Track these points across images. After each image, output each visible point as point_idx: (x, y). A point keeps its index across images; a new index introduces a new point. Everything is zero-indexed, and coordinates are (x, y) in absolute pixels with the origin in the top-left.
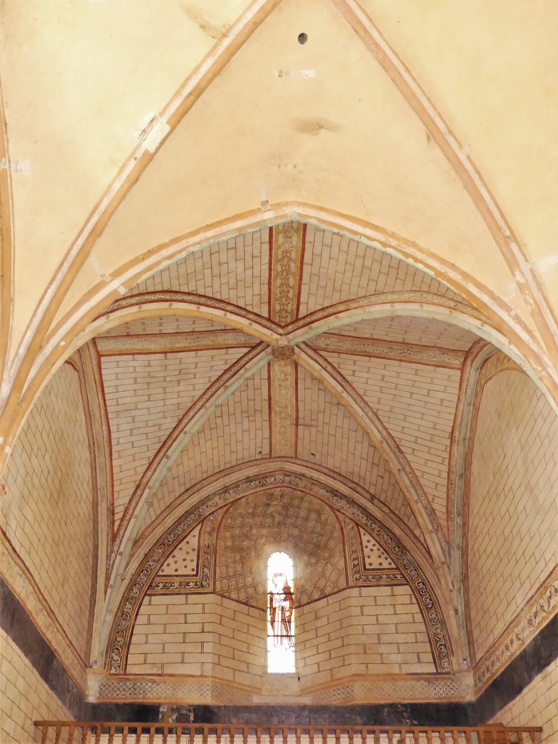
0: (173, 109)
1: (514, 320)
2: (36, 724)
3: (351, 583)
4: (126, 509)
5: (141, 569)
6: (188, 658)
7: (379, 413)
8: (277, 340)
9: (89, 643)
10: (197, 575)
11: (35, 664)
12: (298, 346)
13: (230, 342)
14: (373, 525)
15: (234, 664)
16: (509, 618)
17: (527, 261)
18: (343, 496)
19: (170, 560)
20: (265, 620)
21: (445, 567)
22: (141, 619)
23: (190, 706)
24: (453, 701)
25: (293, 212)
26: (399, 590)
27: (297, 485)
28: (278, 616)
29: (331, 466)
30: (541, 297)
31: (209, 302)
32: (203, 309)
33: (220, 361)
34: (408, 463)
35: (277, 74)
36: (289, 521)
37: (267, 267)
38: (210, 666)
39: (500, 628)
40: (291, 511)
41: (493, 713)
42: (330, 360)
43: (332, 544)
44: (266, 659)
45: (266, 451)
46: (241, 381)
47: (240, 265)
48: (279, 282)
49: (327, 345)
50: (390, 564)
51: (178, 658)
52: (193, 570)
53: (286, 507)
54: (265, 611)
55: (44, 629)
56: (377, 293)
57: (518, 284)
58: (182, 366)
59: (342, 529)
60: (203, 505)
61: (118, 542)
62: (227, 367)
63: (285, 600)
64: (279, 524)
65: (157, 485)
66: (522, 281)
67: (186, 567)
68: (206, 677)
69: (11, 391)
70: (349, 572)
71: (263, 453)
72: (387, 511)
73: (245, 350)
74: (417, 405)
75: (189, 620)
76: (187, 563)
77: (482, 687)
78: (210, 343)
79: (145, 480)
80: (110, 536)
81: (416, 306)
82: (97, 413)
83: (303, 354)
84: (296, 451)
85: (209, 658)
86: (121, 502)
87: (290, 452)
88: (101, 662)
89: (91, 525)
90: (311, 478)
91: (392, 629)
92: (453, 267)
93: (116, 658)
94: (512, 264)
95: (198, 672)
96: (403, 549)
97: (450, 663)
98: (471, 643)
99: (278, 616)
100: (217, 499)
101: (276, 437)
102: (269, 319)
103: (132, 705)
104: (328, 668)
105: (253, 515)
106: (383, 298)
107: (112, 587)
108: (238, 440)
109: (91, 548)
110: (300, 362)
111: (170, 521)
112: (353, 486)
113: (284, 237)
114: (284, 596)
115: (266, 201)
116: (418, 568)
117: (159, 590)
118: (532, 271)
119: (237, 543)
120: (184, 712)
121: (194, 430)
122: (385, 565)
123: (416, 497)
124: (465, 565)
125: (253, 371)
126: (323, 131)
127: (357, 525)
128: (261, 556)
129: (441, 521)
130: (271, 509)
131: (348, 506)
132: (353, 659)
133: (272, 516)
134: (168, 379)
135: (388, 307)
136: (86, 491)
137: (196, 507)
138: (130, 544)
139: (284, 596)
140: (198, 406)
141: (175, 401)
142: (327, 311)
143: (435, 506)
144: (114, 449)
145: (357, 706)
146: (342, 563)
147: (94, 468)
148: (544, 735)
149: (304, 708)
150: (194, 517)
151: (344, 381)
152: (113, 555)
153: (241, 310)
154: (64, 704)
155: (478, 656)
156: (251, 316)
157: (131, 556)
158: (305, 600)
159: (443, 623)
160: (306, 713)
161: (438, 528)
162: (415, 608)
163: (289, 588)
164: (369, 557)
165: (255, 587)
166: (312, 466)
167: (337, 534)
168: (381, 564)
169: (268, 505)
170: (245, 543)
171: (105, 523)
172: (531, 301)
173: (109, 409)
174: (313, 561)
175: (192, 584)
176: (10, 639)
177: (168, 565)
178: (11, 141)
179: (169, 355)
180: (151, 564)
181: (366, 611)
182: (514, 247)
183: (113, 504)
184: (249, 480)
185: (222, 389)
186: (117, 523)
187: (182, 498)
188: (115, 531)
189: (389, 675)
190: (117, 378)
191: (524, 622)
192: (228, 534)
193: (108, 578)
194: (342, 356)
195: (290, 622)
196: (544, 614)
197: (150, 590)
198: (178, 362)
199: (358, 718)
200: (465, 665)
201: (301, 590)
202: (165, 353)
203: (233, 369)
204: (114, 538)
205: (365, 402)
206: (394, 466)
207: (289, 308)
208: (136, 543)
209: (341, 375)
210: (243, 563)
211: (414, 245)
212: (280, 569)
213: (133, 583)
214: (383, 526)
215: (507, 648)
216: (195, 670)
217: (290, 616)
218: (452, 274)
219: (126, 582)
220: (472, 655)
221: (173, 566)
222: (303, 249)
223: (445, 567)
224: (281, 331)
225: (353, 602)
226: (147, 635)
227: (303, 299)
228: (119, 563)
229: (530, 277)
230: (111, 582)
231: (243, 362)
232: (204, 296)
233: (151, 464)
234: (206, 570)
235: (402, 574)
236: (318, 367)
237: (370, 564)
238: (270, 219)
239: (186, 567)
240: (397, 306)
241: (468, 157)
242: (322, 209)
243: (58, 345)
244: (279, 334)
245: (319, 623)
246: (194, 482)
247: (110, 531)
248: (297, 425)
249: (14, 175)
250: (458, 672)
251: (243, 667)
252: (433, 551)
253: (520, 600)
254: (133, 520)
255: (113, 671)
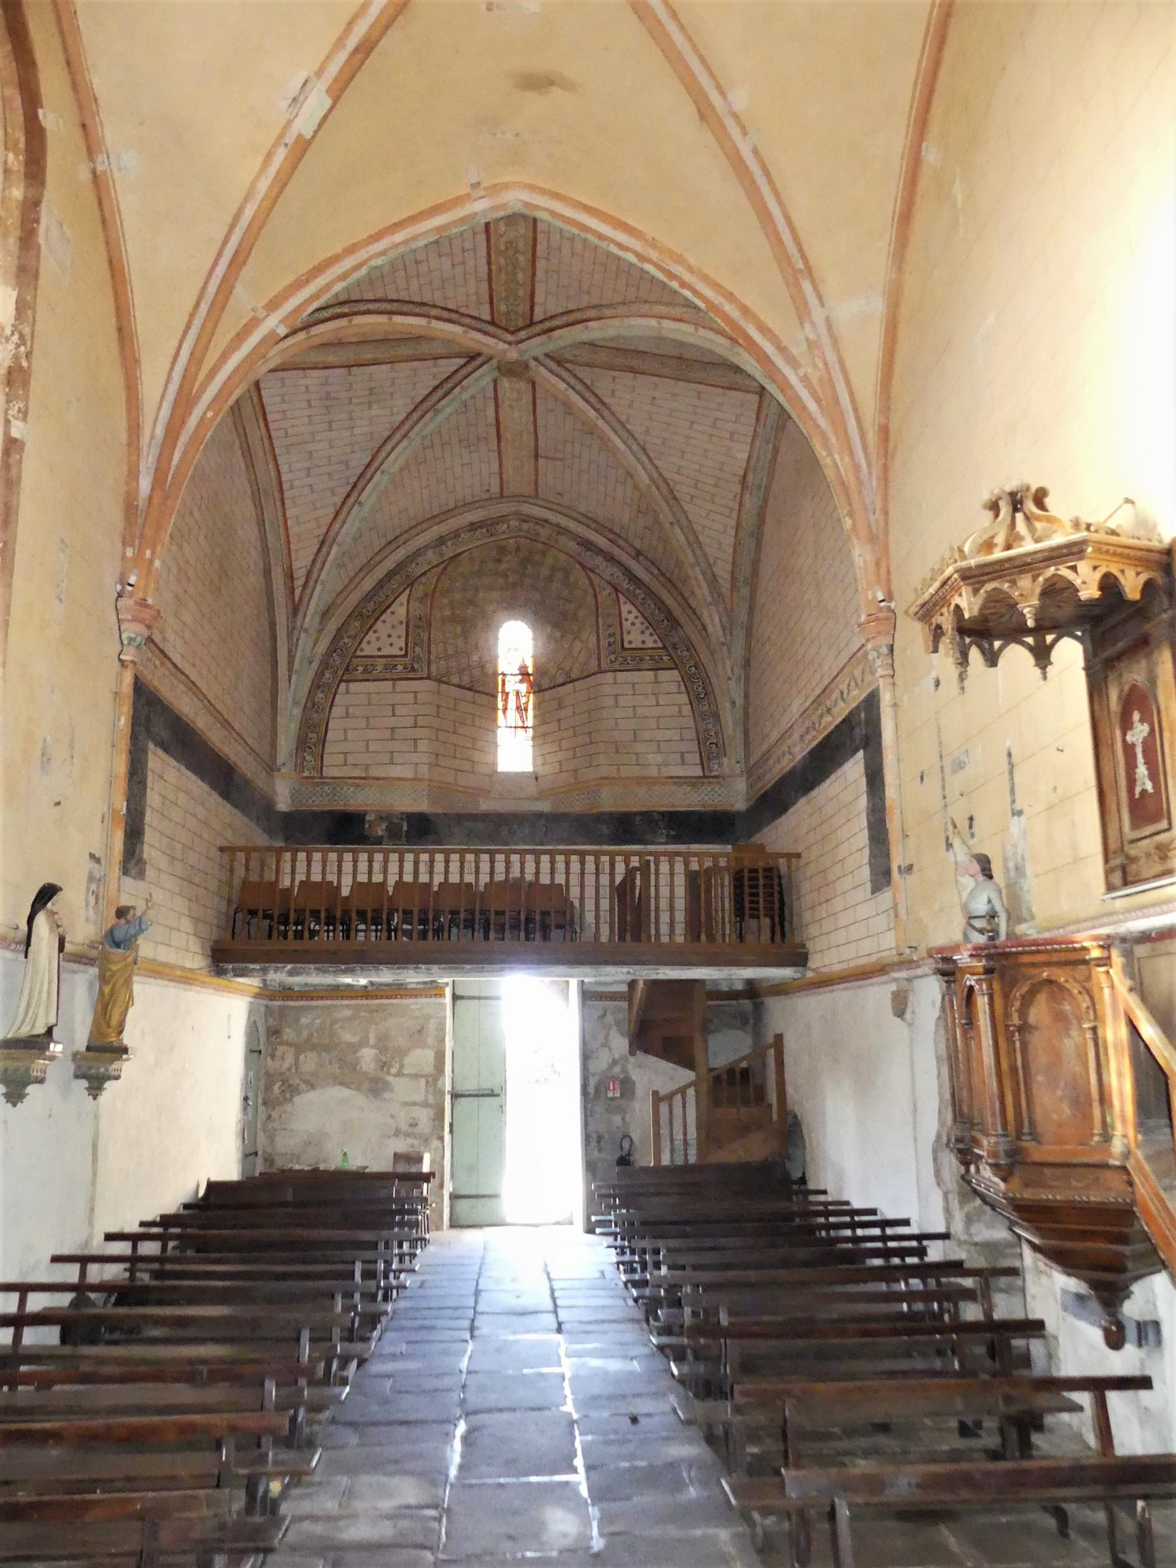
0: (333, 69)
1: (801, 381)
2: (222, 849)
3: (604, 666)
4: (309, 574)
5: (333, 649)
6: (398, 758)
7: (647, 446)
8: (504, 352)
9: (274, 744)
10: (406, 655)
11: (214, 786)
12: (536, 359)
13: (439, 351)
14: (638, 591)
15: (457, 763)
16: (784, 726)
17: (823, 306)
18: (600, 551)
19: (371, 636)
20: (495, 709)
21: (725, 648)
22: (336, 711)
23: (402, 813)
24: (719, 808)
25: (515, 199)
26: (664, 675)
27: (538, 534)
28: (512, 703)
29: (582, 510)
30: (835, 359)
31: (405, 308)
32: (398, 319)
33: (429, 375)
34: (685, 512)
35: (484, 7)
36: (528, 581)
37: (484, 261)
38: (426, 767)
39: (775, 735)
40: (530, 570)
41: (759, 828)
42: (580, 375)
43: (582, 613)
44: (495, 755)
45: (495, 489)
46: (456, 405)
47: (446, 264)
48: (503, 277)
49: (575, 356)
50: (655, 642)
51: (385, 758)
52: (401, 649)
53: (524, 563)
54: (495, 697)
55: (218, 744)
56: (638, 301)
57: (807, 339)
58: (372, 385)
59: (595, 596)
60: (412, 562)
61: (300, 616)
62: (436, 383)
63: (521, 681)
64: (514, 585)
65: (349, 540)
66: (812, 337)
67: (391, 645)
68: (420, 780)
69: (152, 489)
70: (603, 653)
71: (492, 490)
72: (656, 572)
73: (462, 361)
74: (698, 445)
75: (397, 712)
76: (393, 639)
77: (831, 723)
78: (410, 352)
79: (331, 534)
80: (290, 607)
81: (690, 328)
82: (260, 453)
83: (542, 369)
84: (537, 489)
85: (425, 759)
86: (301, 563)
87: (528, 490)
88: (290, 765)
89: (265, 600)
90: (558, 525)
91: (652, 723)
92: (731, 297)
93: (308, 758)
94: (802, 313)
95: (410, 775)
96: (674, 623)
97: (720, 765)
98: (747, 743)
99: (512, 703)
100: (430, 553)
101: (509, 470)
102: (492, 323)
103: (331, 812)
104: (573, 767)
105: (479, 574)
106: (645, 308)
107: (297, 671)
108: (458, 474)
109: (267, 628)
110: (538, 380)
111: (369, 584)
112: (611, 536)
113: (506, 226)
114: (520, 677)
115: (475, 185)
116: (690, 646)
117: (358, 674)
118: (827, 319)
119: (458, 612)
120: (395, 820)
121: (395, 469)
122: (650, 644)
123: (692, 560)
124: (749, 649)
125: (472, 391)
126: (555, 89)
127: (616, 590)
128: (491, 626)
129: (724, 590)
130: (503, 566)
131: (605, 564)
132: (602, 759)
133: (506, 576)
134: (355, 401)
135: (653, 322)
136: (253, 559)
137: (401, 566)
138: (317, 619)
139: (520, 677)
140: (398, 436)
141: (367, 429)
142: (573, 318)
143: (716, 570)
144: (287, 494)
145: (603, 813)
146: (593, 638)
147: (261, 524)
148: (802, 862)
149: (540, 815)
150: (401, 577)
151: (600, 406)
152: (296, 632)
153: (452, 315)
154: (251, 819)
155: (752, 761)
156: (467, 321)
157: (320, 631)
158: (546, 683)
159: (716, 716)
160: (542, 822)
161: (718, 597)
162: (684, 699)
163: (526, 667)
164: (629, 633)
165: (483, 667)
166: (560, 509)
167: (590, 600)
168: (644, 642)
169: (499, 561)
170: (469, 611)
171: (281, 594)
172: (821, 365)
173: (276, 443)
174: (558, 634)
175: (400, 668)
176: (183, 768)
177: (369, 643)
178: (106, 127)
179: (354, 369)
180: (346, 641)
181: (621, 701)
182: (807, 286)
183: (291, 568)
184: (473, 527)
185: (430, 414)
186: (298, 592)
187: (385, 553)
188: (297, 599)
189: (646, 778)
190: (283, 401)
191: (796, 737)
192: (445, 601)
193: (291, 662)
194: (596, 370)
195: (526, 710)
196: (814, 733)
197: (347, 675)
198: (366, 377)
199: (605, 827)
200: (738, 769)
201: (540, 669)
202: (350, 366)
203: (445, 387)
204: (295, 610)
205: (628, 431)
206: (666, 516)
207: (520, 309)
208: (325, 615)
209: (596, 395)
210: (466, 638)
211: (680, 260)
212: (515, 644)
213: (325, 664)
214: (649, 592)
215: (779, 761)
216: (409, 773)
217: (527, 703)
218: (728, 308)
219: (315, 666)
220: (747, 755)
221: (375, 645)
222: (535, 239)
223: (725, 648)
224: (510, 338)
225: (607, 689)
226: (345, 730)
227: (539, 299)
228: (305, 641)
229: (823, 330)
230: (296, 666)
231: (458, 377)
232: (397, 301)
233: (337, 513)
234: (417, 649)
235: (669, 655)
236: (563, 386)
237: (630, 642)
238: (484, 212)
239: (391, 645)
240: (666, 324)
241: (755, 151)
242: (556, 196)
243: (203, 417)
244: (505, 342)
245: (563, 713)
246: (398, 533)
247: (290, 602)
248: (537, 456)
249: (116, 175)
250: (730, 776)
251: (466, 766)
252: (710, 629)
253: (796, 708)
254: (319, 587)
255: (306, 774)
